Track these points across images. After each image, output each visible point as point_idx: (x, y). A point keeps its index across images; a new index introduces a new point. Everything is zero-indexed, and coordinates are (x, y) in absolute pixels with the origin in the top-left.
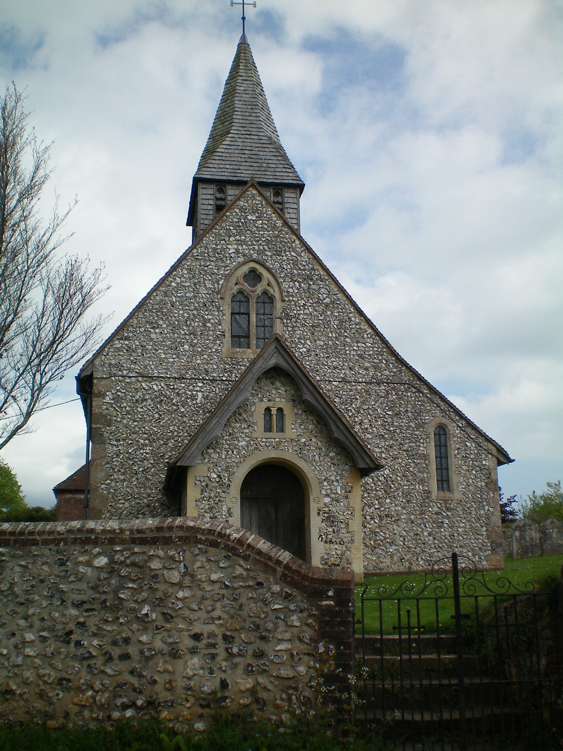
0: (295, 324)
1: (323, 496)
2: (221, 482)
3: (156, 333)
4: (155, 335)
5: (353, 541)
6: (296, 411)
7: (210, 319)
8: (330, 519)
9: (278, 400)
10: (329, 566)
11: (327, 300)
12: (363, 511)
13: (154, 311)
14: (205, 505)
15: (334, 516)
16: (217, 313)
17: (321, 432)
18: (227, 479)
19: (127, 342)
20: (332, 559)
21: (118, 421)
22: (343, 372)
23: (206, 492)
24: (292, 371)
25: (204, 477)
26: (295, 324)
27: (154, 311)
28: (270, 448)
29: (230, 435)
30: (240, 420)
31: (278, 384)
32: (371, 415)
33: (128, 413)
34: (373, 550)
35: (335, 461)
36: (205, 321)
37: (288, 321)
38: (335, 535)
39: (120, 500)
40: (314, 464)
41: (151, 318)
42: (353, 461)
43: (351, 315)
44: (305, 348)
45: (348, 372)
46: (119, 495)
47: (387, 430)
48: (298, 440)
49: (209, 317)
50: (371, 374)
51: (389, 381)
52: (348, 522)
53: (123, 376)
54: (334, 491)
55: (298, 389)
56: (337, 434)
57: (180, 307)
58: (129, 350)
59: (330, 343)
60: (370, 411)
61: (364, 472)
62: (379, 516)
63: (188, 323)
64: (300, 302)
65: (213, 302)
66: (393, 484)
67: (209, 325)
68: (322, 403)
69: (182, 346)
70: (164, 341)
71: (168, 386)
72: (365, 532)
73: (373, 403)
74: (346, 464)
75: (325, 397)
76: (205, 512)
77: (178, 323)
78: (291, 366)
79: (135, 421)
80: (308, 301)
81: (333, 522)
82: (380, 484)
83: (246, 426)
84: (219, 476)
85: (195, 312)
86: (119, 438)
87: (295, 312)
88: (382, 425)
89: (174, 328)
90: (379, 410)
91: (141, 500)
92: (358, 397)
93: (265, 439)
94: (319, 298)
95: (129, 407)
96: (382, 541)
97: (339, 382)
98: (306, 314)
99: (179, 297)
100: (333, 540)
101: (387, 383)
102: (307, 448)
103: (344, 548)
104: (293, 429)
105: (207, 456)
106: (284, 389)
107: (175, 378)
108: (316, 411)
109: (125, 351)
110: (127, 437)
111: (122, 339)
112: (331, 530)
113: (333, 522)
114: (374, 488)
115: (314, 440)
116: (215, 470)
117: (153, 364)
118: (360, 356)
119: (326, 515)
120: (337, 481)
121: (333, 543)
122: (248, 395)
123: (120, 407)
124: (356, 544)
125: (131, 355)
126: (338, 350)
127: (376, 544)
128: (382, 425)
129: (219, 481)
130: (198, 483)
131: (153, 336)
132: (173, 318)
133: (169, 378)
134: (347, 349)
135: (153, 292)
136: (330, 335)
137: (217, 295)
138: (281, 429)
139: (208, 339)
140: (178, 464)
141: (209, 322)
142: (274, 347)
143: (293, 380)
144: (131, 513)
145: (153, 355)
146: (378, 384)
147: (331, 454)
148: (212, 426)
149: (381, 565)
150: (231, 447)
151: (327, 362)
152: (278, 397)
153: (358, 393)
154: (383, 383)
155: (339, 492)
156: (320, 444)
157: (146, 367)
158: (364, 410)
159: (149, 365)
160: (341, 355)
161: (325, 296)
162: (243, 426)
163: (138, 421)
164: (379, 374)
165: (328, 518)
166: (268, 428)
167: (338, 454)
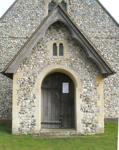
0: (75, 14)
1: (83, 88)
2: (30, 81)
3: (17, 20)
4: (16, 20)
5: (98, 111)
6: (69, 45)
7: (39, 13)
8: (87, 100)
9: (60, 39)
10: (86, 124)
11: (90, 4)
12: (104, 92)
13: (16, 10)
14: (22, 92)
15: (89, 98)
16: (42, 11)
17: (82, 55)
18: (33, 80)
19: (5, 24)
20: (88, 121)
21: (1, 56)
22: (96, 34)
23: (22, 86)
24: (67, 23)
25: (21, 79)
26: (75, 14)
27: (16, 10)
28: (55, 64)
29: (35, 57)
30: (40, 50)
31: (60, 31)
32: (108, 52)
33: (5, 53)
34: (108, 109)
35: (90, 70)
36: (37, 14)
37: (73, 13)
38: (89, 108)
39: (2, 88)
40: (79, 72)
41: (15, 13)
42: (99, 70)
43: (100, 10)
44: (79, 24)
45: (98, 34)
46: (1, 86)
47: (115, 58)
48: (70, 60)
49: (39, 12)
50: (108, 35)
51: (116, 37)
52: (96, 101)
53: (3, 38)
54: (89, 86)
55: (71, 33)
56: (91, 56)
57: (27, 9)
58: (6, 27)
59: (91, 22)
60: (108, 50)
61: (105, 76)
62: (111, 94)
63: (30, 15)
64: (78, 5)
65: (41, 6)
66: (117, 81)
67: (39, 15)
68: (85, 42)
69: (27, 25)
70: (20, 23)
71: (21, 41)
72: (105, 101)
73: (109, 47)
74: (96, 72)
75: (84, 36)
76: (22, 96)
77: (26, 15)
78: (66, 20)
79: (8, 56)
80: (81, 4)
81: (88, 101)
82: (111, 81)
83: (43, 53)
84: (29, 78)
85: (33, 10)
86: (2, 63)
87: (75, 9)
88: (113, 56)
89: (24, 18)
90: (111, 50)
91: (10, 88)
92: (102, 44)
93: (53, 59)
94: (86, 3)
95: (6, 50)
96: (112, 105)
97: (94, 38)
98: (80, 10)
99: (26, 4)
100: (88, 111)
101: (115, 38)
102: (75, 63)
103: (94, 115)
104: (68, 54)
105: (23, 68)
106: (63, 34)
107: (25, 38)
108: (80, 45)
109: (4, 27)
110: (5, 63)
111: (3, 22)
112: (87, 105)
113: (88, 101)
114: (109, 83)
115: (79, 59)
116: (27, 75)
117: (15, 32)
118: (104, 27)
119: (85, 98)
120: (91, 80)
121: (88, 112)
122: (43, 36)
123: (2, 50)
124: (100, 113)
125: (6, 29)
126: (94, 25)
127: (109, 106)
128: (113, 56)
129: (29, 81)
130: (18, 82)
131: (16, 21)
132: (24, 13)
133: (22, 38)
134: (98, 24)
135: (16, 3)
136: (91, 18)
137: (42, 3)
138: (62, 54)
139: (38, 22)
140: (6, 72)
141: (39, 14)
142: (57, 11)
143: (68, 29)
144: (6, 93)
145: (15, 29)
146: (111, 39)
147: (88, 67)
148: (24, 52)
149: (112, 115)
150: (35, 63)
151: (89, 30)
152: (60, 38)
153: (102, 42)
154: (113, 38)
155: (92, 86)
156: (82, 61)
157: (12, 34)
158: (105, 50)
159: (14, 33)
160: (95, 26)
161: (88, 2)
162: (42, 53)
163: (9, 56)
164: (112, 35)
165: (85, 99)
166: (55, 54)
167: (91, 66)
